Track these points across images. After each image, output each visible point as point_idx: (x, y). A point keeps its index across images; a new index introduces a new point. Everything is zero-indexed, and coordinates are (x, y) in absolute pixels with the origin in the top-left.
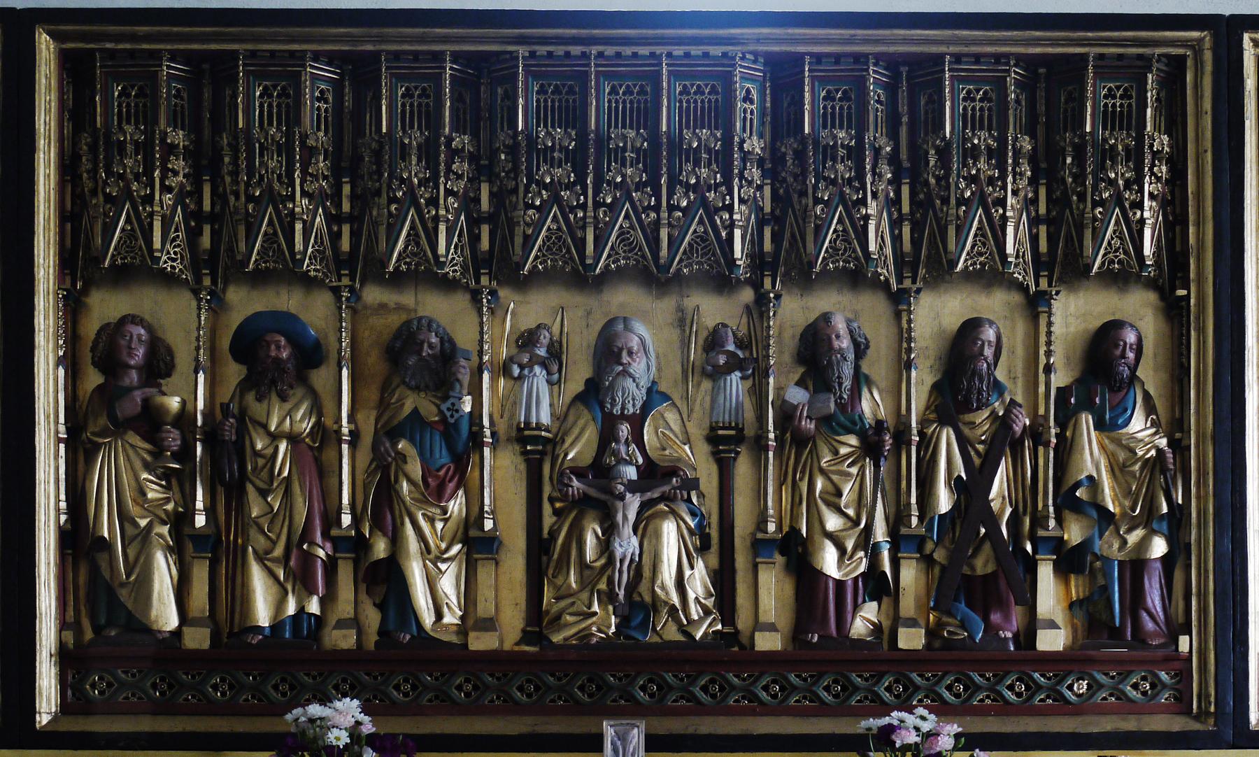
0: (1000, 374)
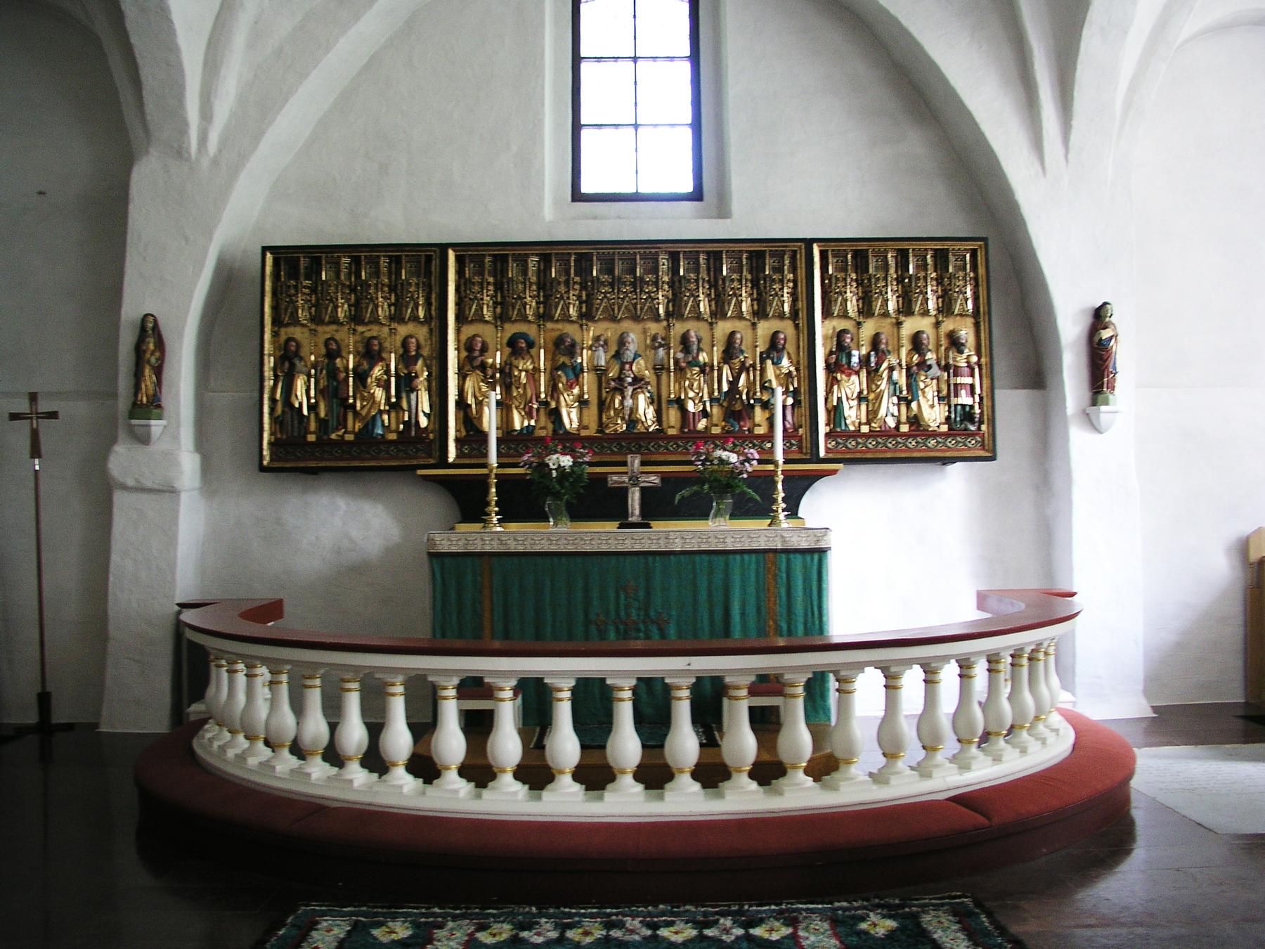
0: (743, 348)
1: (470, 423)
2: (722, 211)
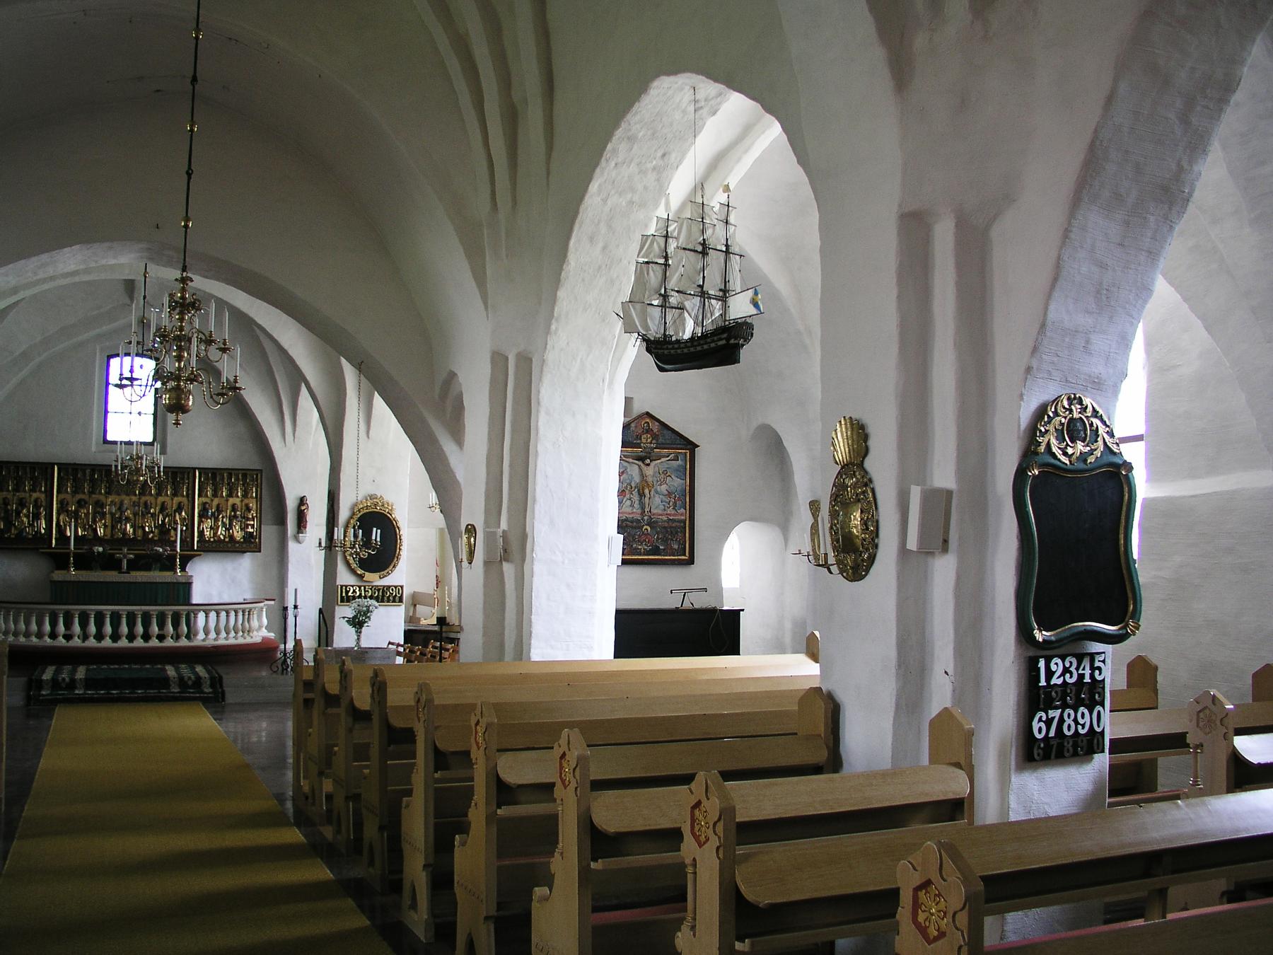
1: (61, 531)
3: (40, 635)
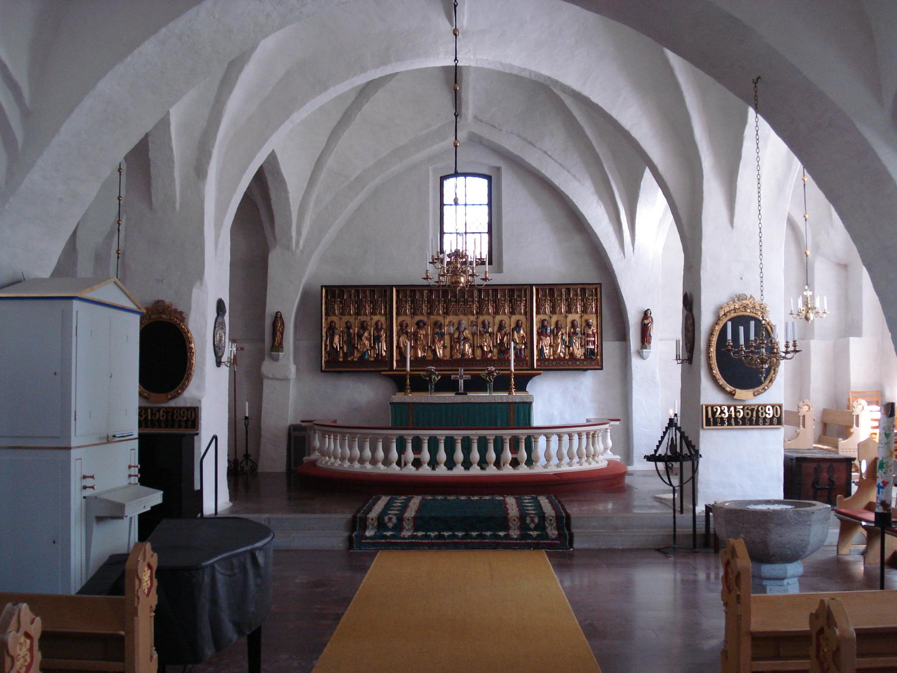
2: (500, 270)
3: (374, 461)
